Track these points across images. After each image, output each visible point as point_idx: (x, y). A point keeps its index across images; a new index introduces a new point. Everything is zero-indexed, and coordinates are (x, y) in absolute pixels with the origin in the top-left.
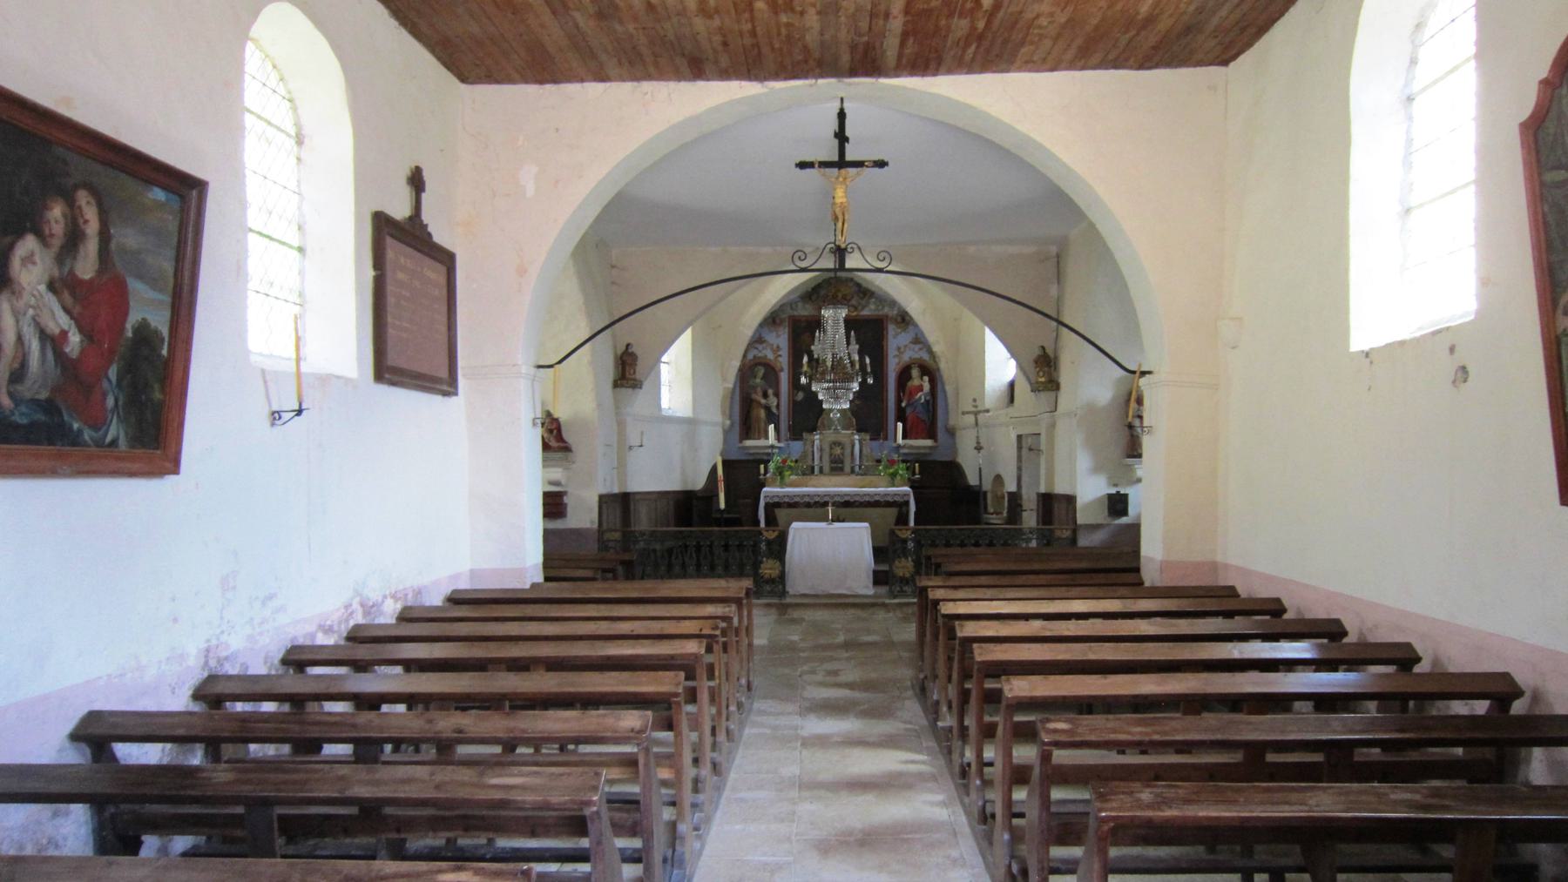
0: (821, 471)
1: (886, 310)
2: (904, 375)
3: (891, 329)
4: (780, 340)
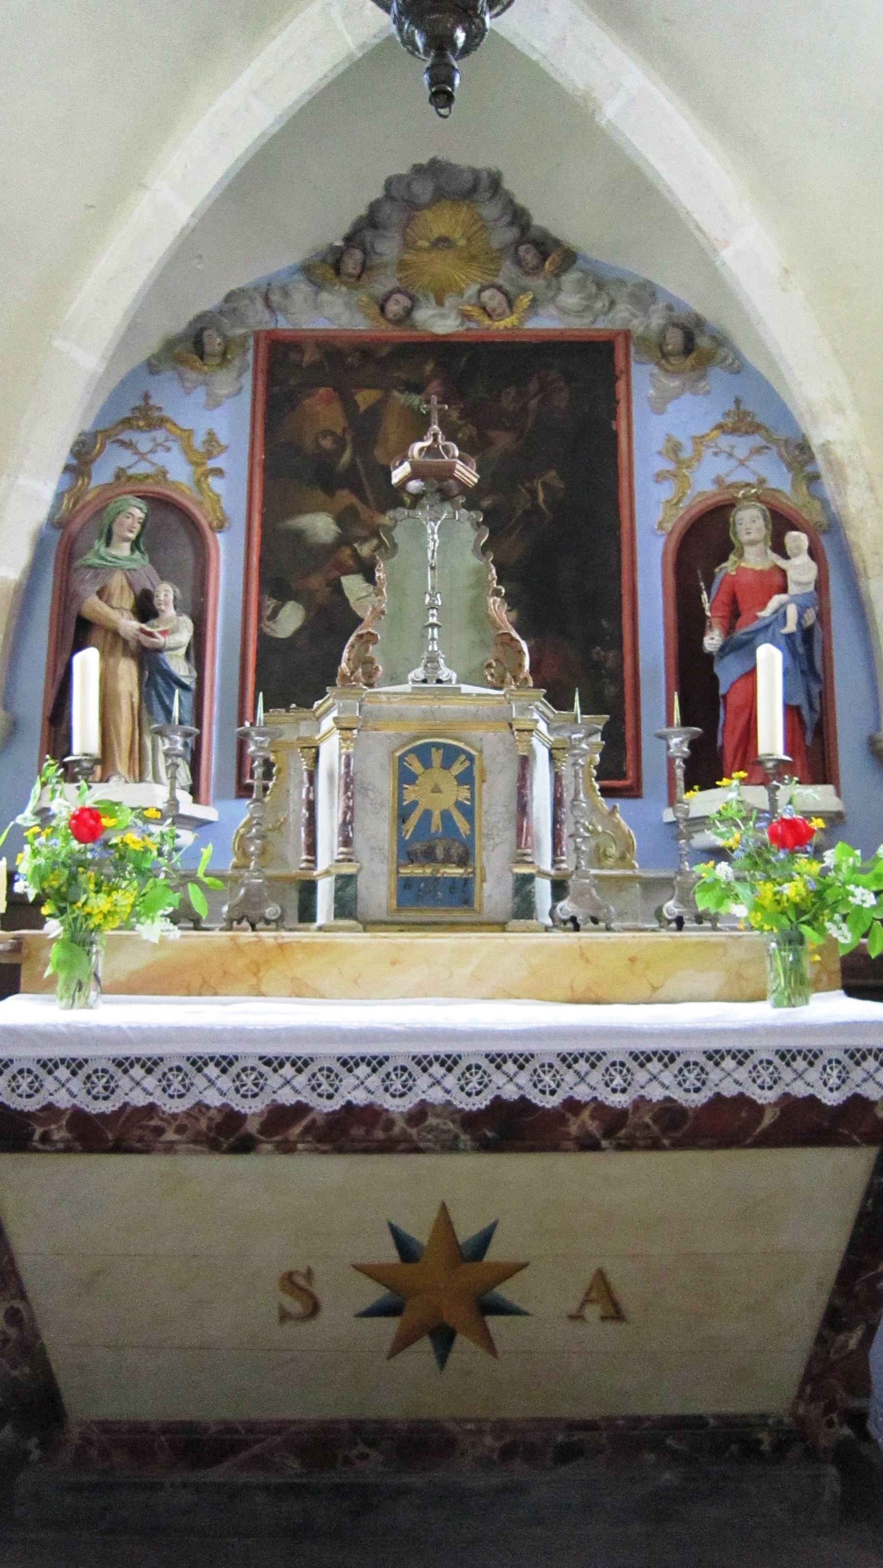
0: (346, 906)
1: (622, 317)
2: (705, 538)
3: (643, 382)
4: (215, 433)
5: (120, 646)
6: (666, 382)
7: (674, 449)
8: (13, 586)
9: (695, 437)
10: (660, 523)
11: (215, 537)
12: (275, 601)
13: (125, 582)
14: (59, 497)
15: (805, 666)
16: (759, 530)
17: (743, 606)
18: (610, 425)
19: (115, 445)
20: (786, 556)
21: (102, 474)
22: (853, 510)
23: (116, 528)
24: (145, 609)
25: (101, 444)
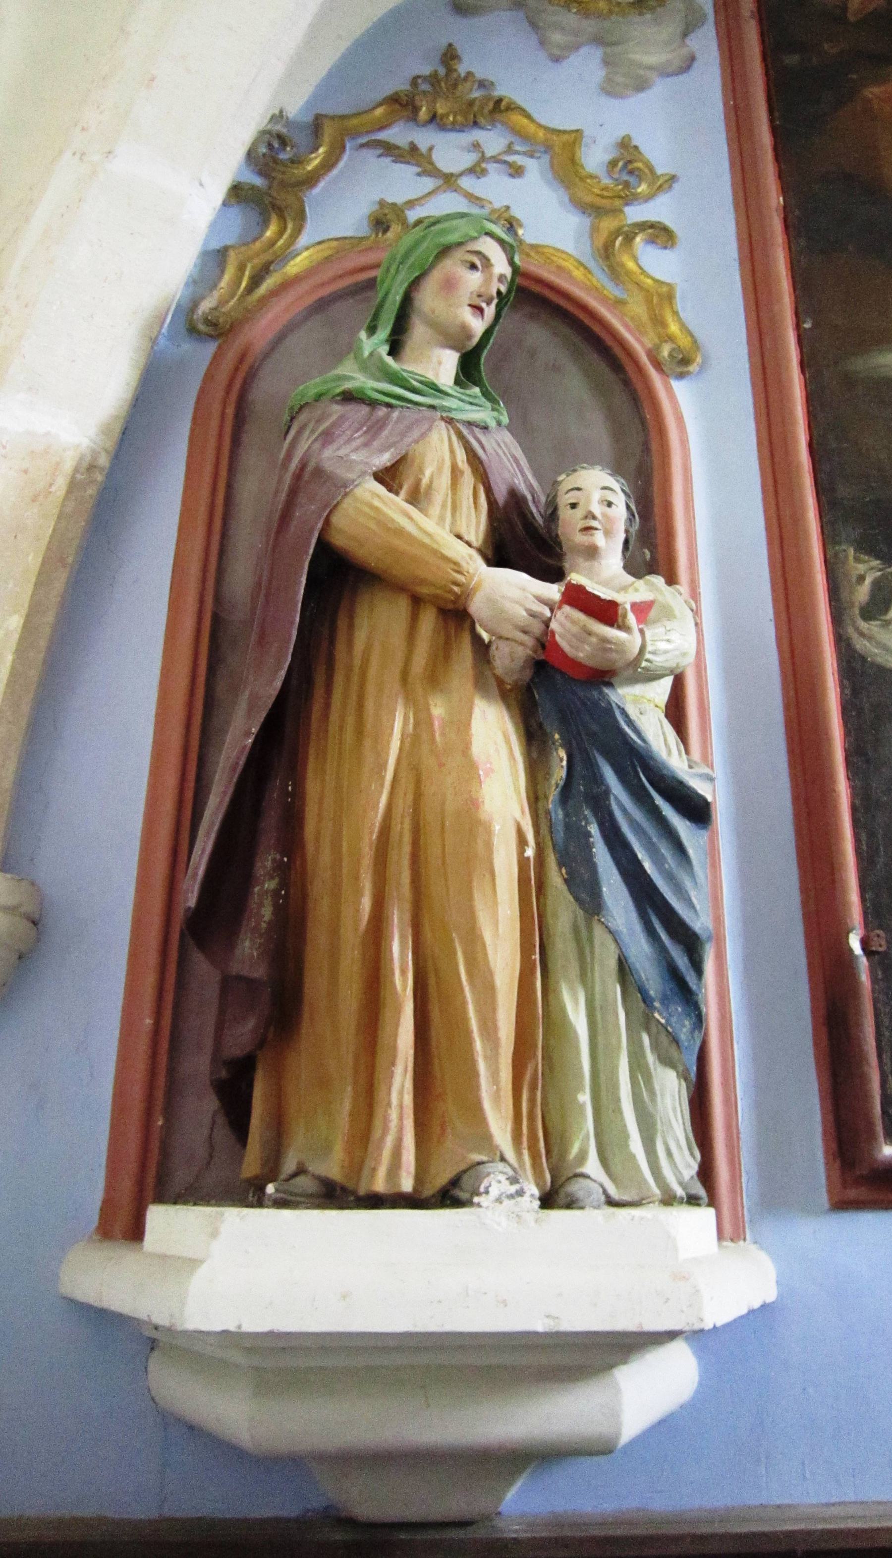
5: (465, 653)
8: (68, 466)
11: (669, 390)
12: (876, 563)
13: (461, 456)
14: (215, 258)
19: (370, 155)
21: (339, 211)
23: (428, 299)
24: (525, 538)
25: (329, 154)
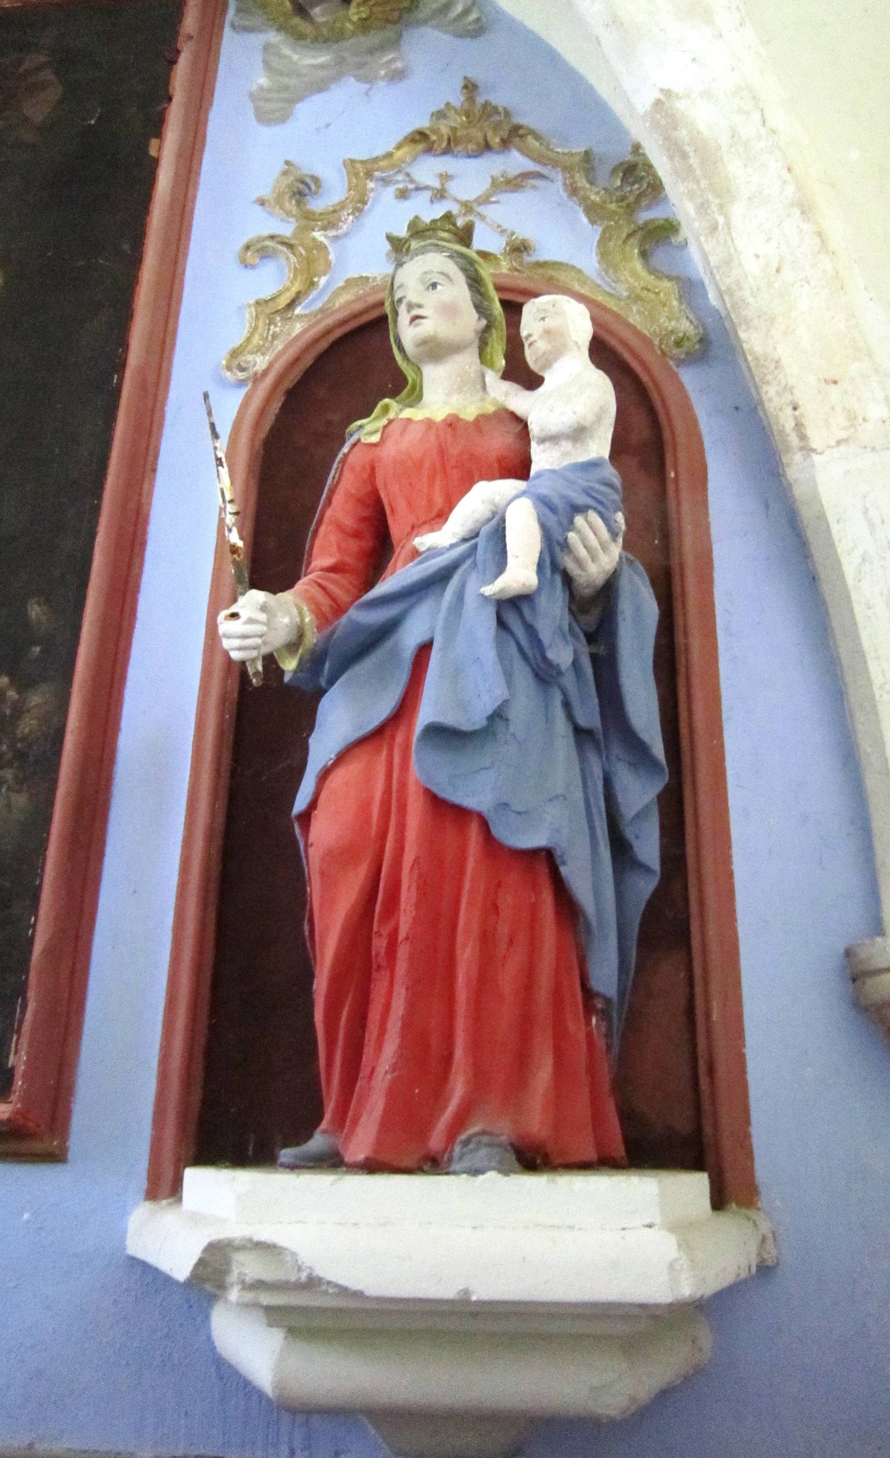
6: (296, 57)
7: (300, 188)
9: (352, 161)
10: (235, 353)
15: (589, 715)
16: (449, 311)
17: (396, 529)
18: (146, 146)
20: (530, 380)
22: (752, 267)
